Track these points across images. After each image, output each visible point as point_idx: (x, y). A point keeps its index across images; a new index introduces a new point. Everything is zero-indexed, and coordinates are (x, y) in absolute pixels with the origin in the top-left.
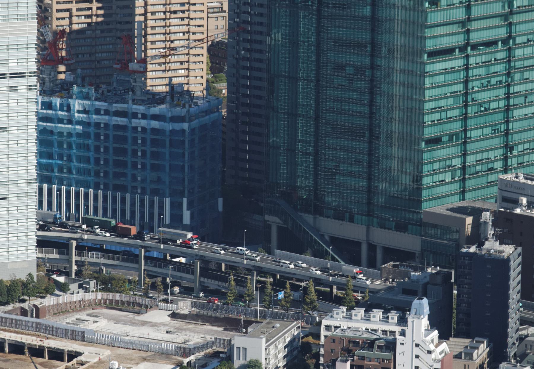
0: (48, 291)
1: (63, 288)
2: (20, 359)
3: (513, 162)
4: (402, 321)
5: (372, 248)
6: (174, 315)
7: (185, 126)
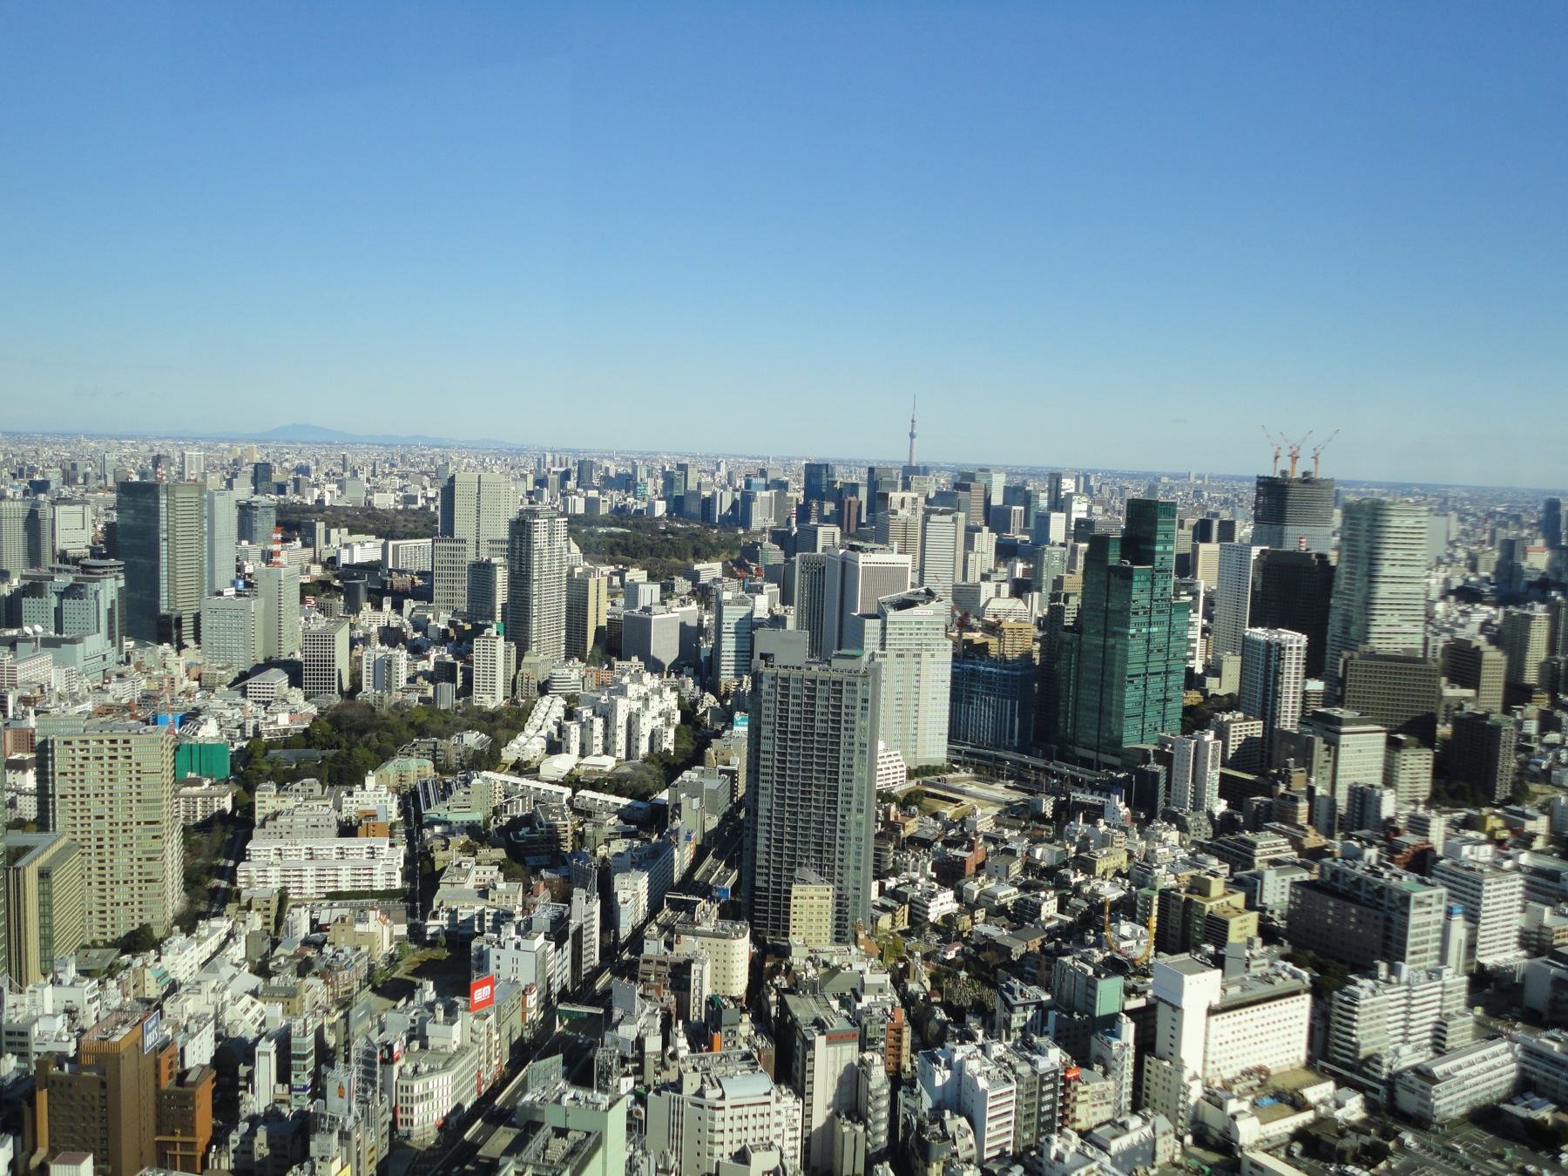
0: (950, 772)
1: (957, 770)
2: (1168, 787)
3: (1166, 728)
4: (1108, 797)
5: (1099, 762)
6: (1007, 787)
7: (1019, 673)
